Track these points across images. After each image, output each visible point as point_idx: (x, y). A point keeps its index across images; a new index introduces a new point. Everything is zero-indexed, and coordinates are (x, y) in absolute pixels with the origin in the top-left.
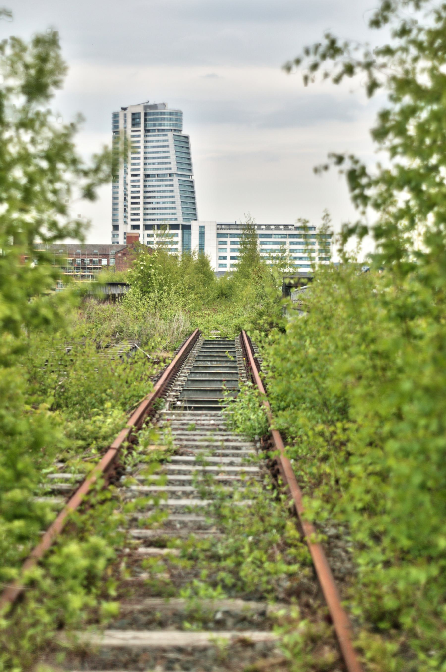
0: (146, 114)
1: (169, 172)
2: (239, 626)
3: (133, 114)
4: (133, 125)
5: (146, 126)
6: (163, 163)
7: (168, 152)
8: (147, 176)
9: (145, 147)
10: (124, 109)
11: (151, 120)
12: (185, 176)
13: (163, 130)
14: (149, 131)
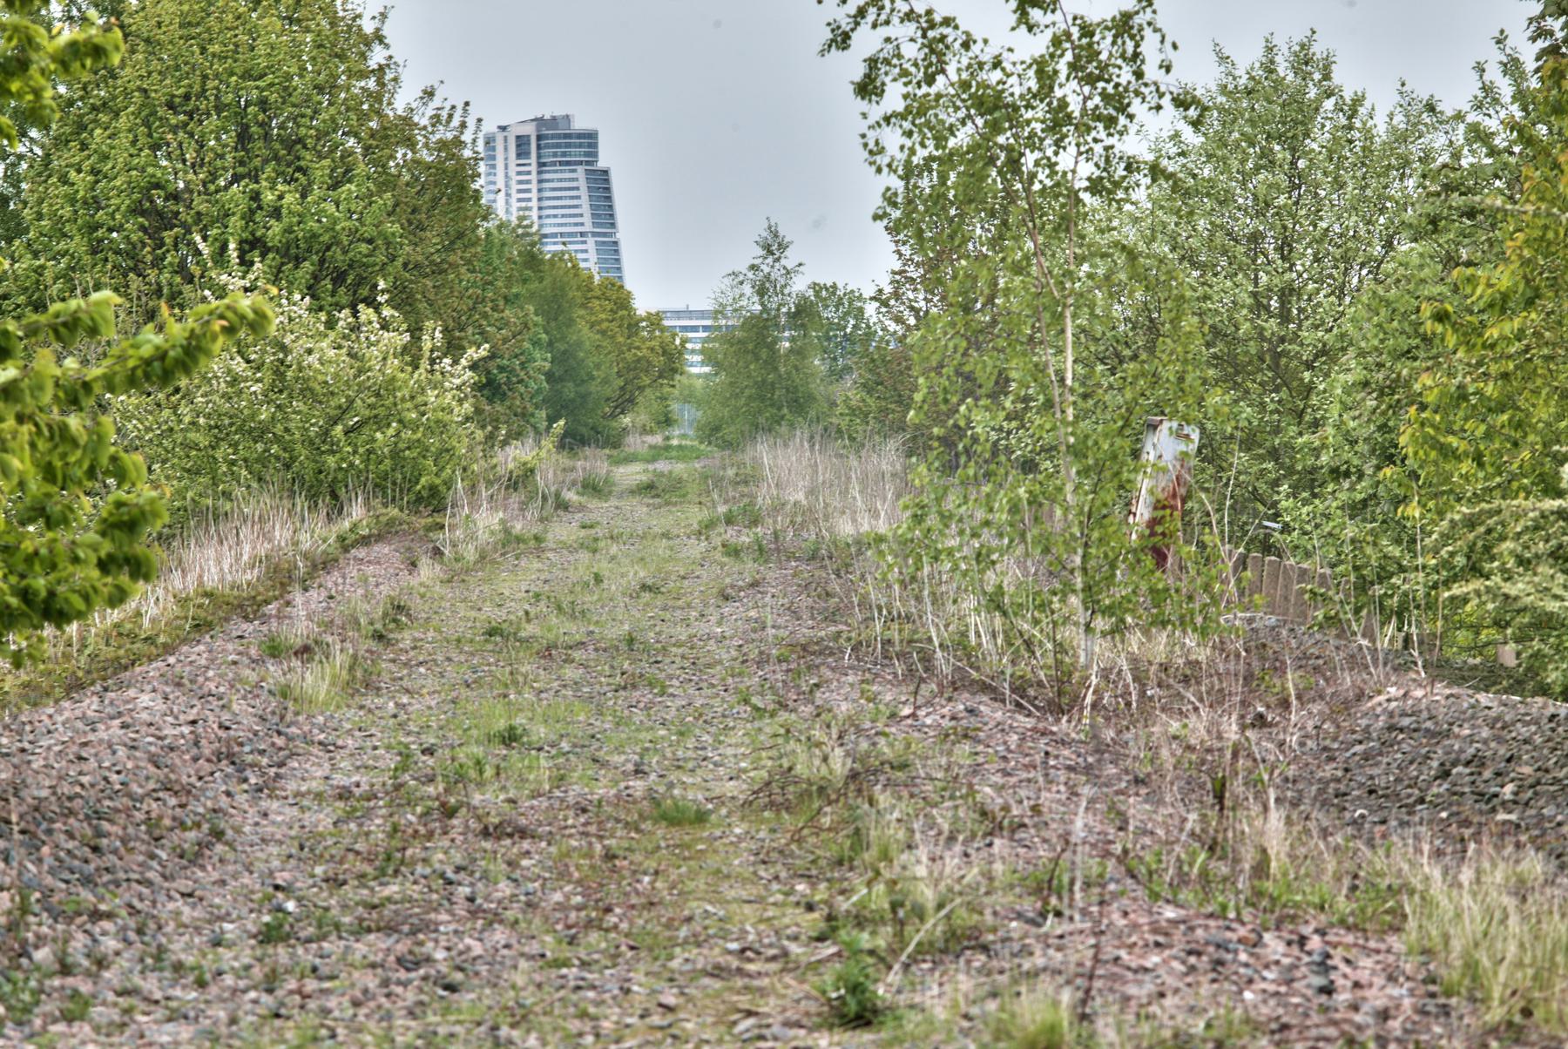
0: (539, 138)
1: (580, 229)
2: (1315, 968)
3: (518, 137)
4: (519, 156)
5: (539, 157)
6: (571, 216)
7: (578, 197)
9: (540, 190)
10: (503, 128)
11: (547, 146)
12: (605, 234)
13: (568, 163)
14: (544, 164)
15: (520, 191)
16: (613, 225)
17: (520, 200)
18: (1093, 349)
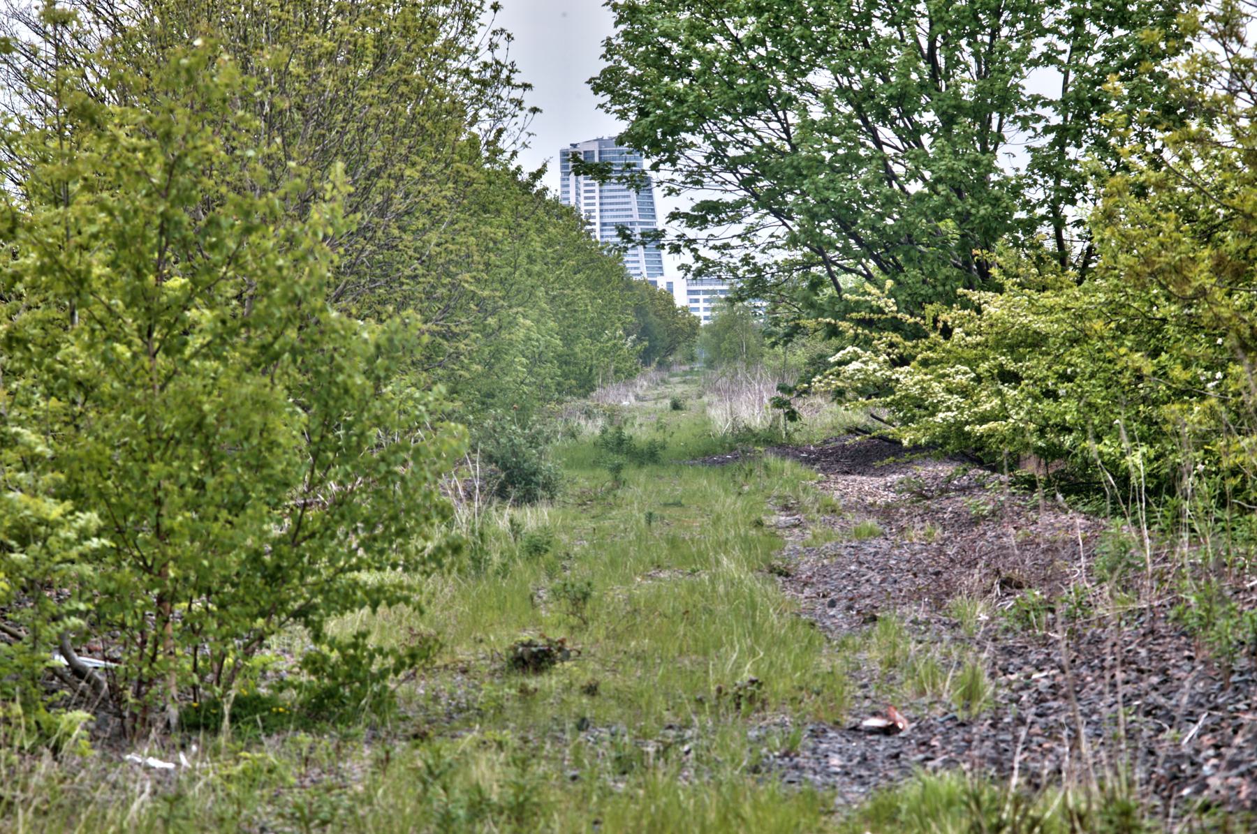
0: (600, 152)
8: (603, 224)
12: (648, 223)
15: (586, 191)
16: (654, 217)
17: (586, 198)
18: (1210, 385)
